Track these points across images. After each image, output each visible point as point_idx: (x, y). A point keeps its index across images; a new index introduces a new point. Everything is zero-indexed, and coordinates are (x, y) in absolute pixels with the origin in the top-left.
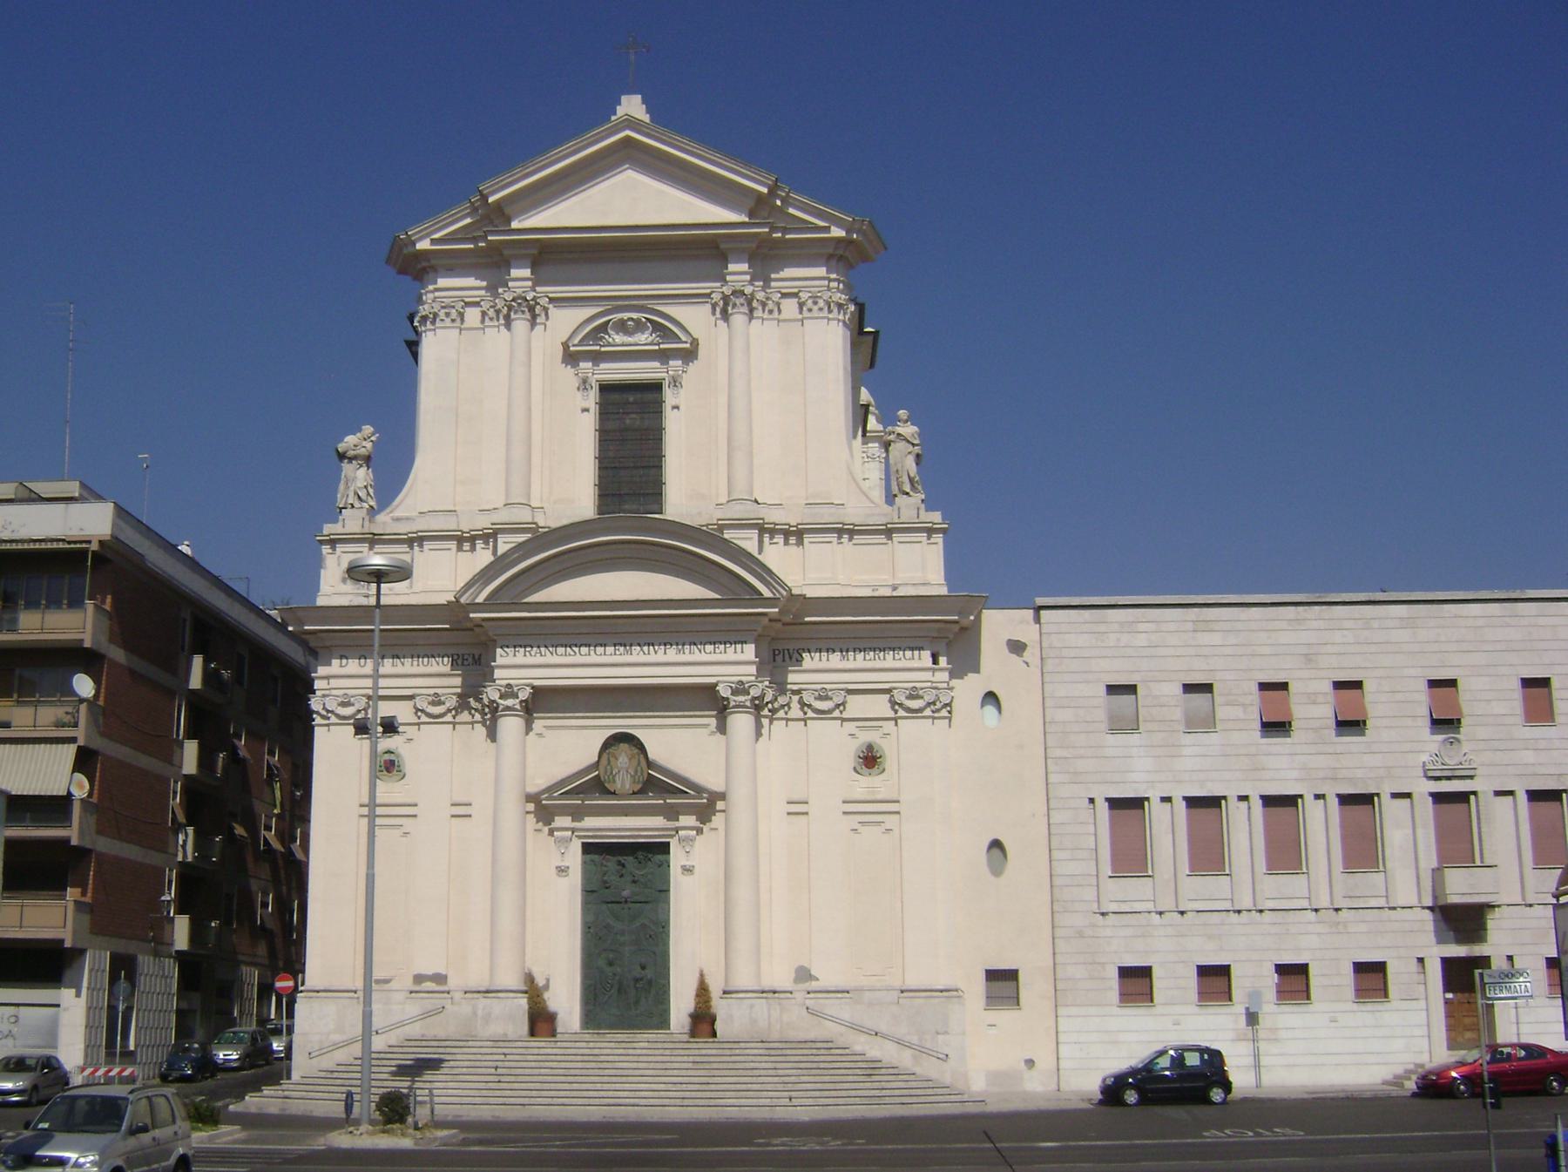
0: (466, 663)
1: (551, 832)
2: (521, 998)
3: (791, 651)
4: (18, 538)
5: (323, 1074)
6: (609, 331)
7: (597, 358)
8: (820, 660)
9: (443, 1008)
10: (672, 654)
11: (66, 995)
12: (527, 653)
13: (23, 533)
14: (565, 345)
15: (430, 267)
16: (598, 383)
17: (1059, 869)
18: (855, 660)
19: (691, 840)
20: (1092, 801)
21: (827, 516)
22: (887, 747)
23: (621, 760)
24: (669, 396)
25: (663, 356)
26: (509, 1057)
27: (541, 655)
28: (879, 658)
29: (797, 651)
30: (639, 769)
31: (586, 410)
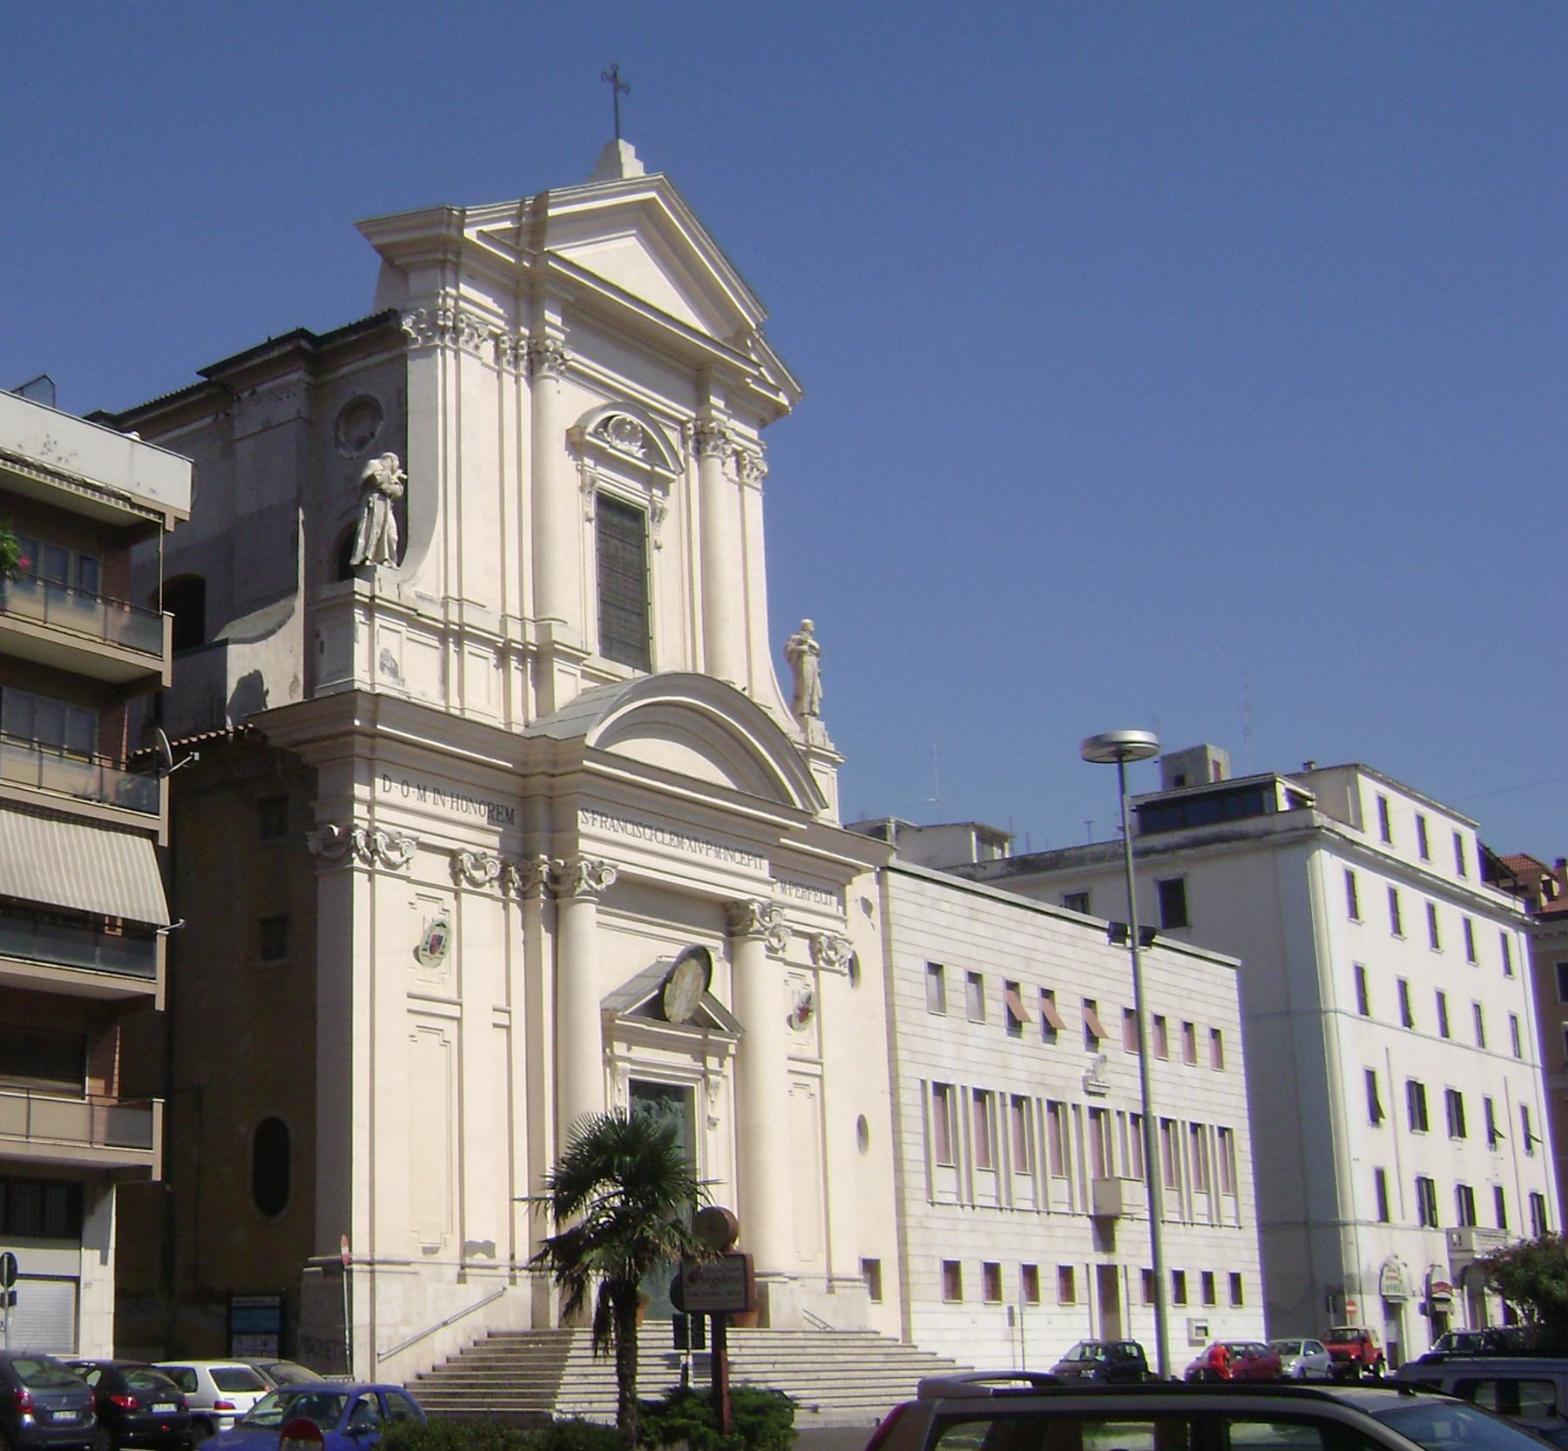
4: (66, 473)
7: (603, 458)
10: (708, 855)
11: (90, 1257)
13: (72, 468)
26: (744, 1351)
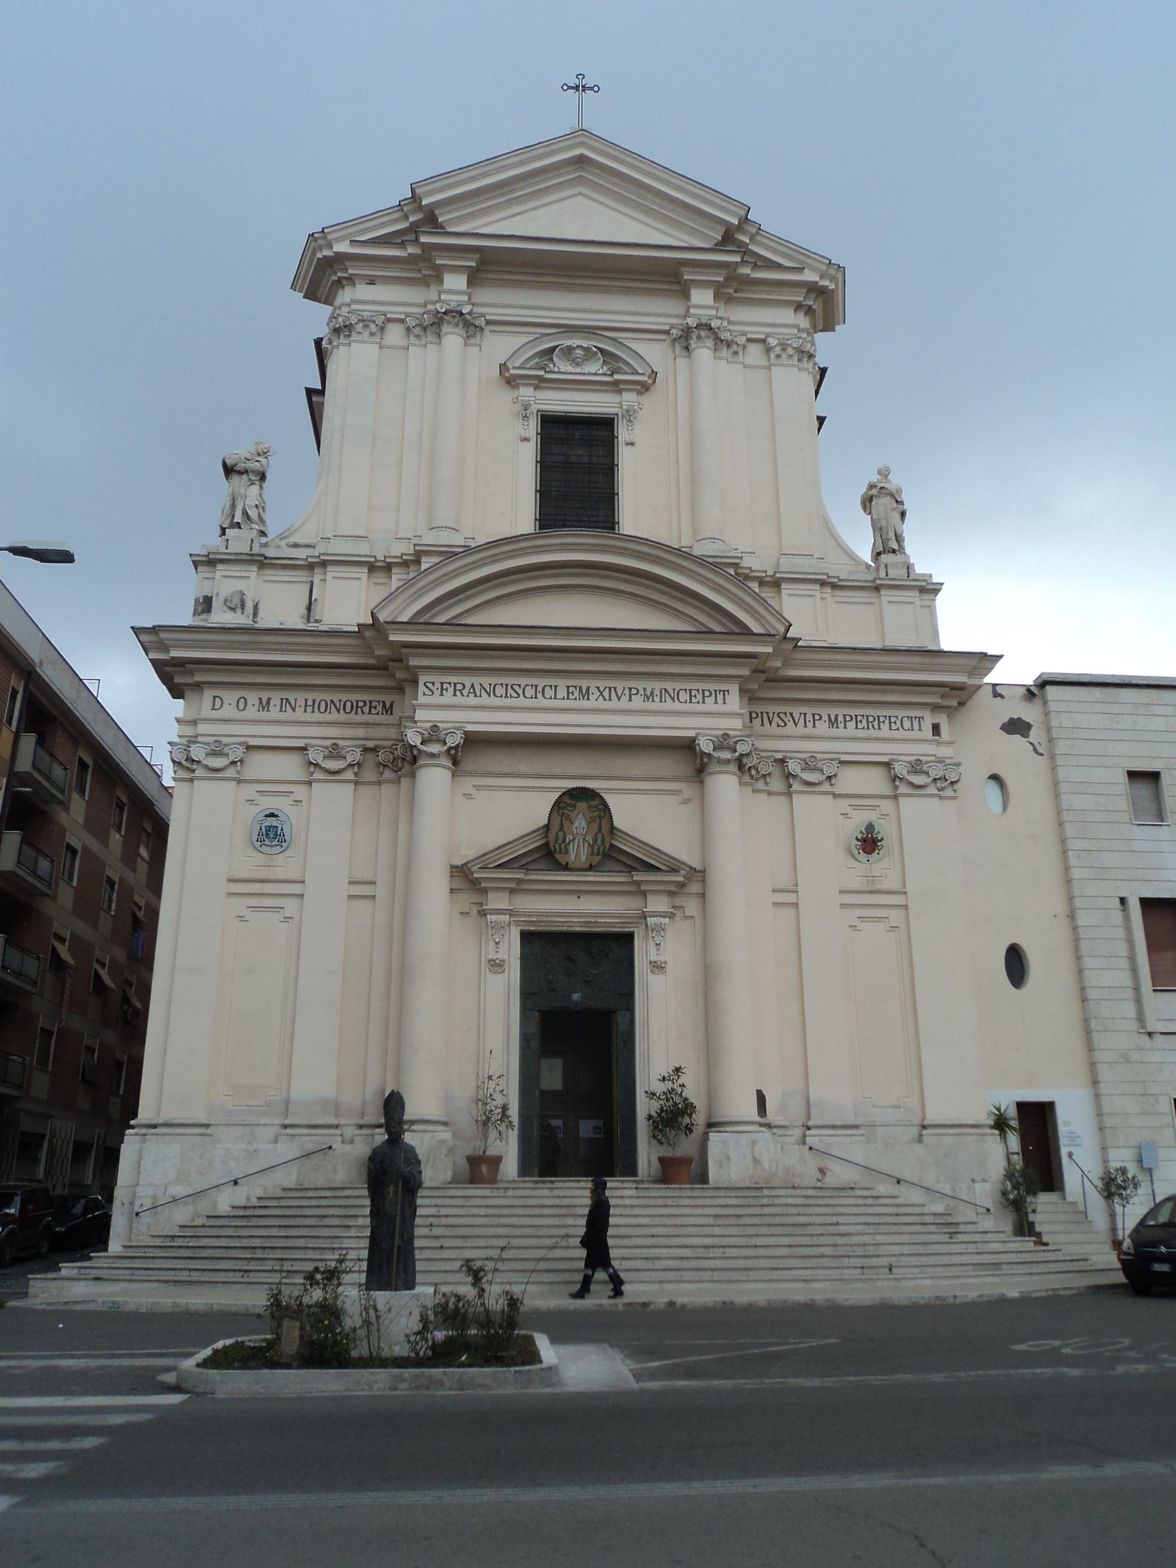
0: (373, 711)
1: (483, 914)
2: (443, 1131)
3: (771, 715)
5: (158, 1242)
6: (555, 358)
7: (540, 383)
8: (805, 726)
9: (330, 1148)
12: (458, 693)
14: (503, 367)
15: (346, 278)
16: (539, 414)
17: (1092, 979)
18: (845, 728)
19: (661, 929)
20: (1123, 901)
21: (806, 566)
22: (885, 829)
23: (576, 824)
24: (623, 433)
25: (616, 387)
27: (476, 696)
28: (873, 726)
29: (778, 715)
30: (599, 836)
31: (526, 439)
